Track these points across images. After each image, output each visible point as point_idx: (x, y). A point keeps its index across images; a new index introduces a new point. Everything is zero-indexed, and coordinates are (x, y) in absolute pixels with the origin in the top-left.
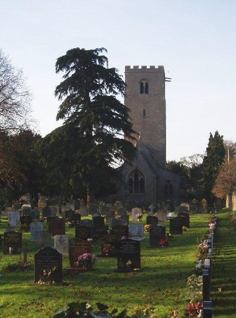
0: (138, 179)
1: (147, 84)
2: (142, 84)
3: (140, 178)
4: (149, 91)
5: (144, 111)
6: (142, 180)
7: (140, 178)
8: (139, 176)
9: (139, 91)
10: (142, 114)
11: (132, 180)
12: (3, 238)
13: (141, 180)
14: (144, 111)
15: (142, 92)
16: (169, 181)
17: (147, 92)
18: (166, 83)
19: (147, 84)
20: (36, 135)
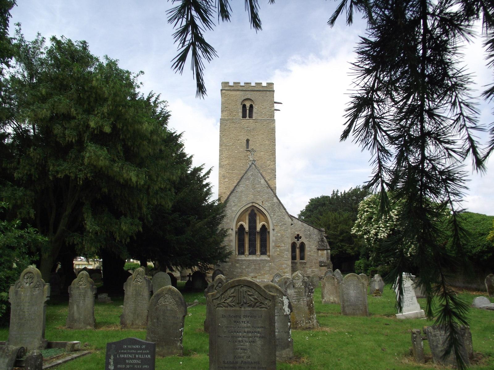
0: (255, 228)
1: (251, 106)
2: (244, 106)
3: (259, 227)
4: (254, 116)
5: (248, 141)
6: (264, 229)
7: (259, 227)
8: (258, 221)
9: (241, 114)
10: (245, 145)
11: (244, 229)
12: (402, 129)
13: (261, 229)
14: (248, 141)
15: (244, 116)
16: (298, 237)
17: (251, 116)
18: (276, 113)
19: (251, 106)
20: (198, 170)
